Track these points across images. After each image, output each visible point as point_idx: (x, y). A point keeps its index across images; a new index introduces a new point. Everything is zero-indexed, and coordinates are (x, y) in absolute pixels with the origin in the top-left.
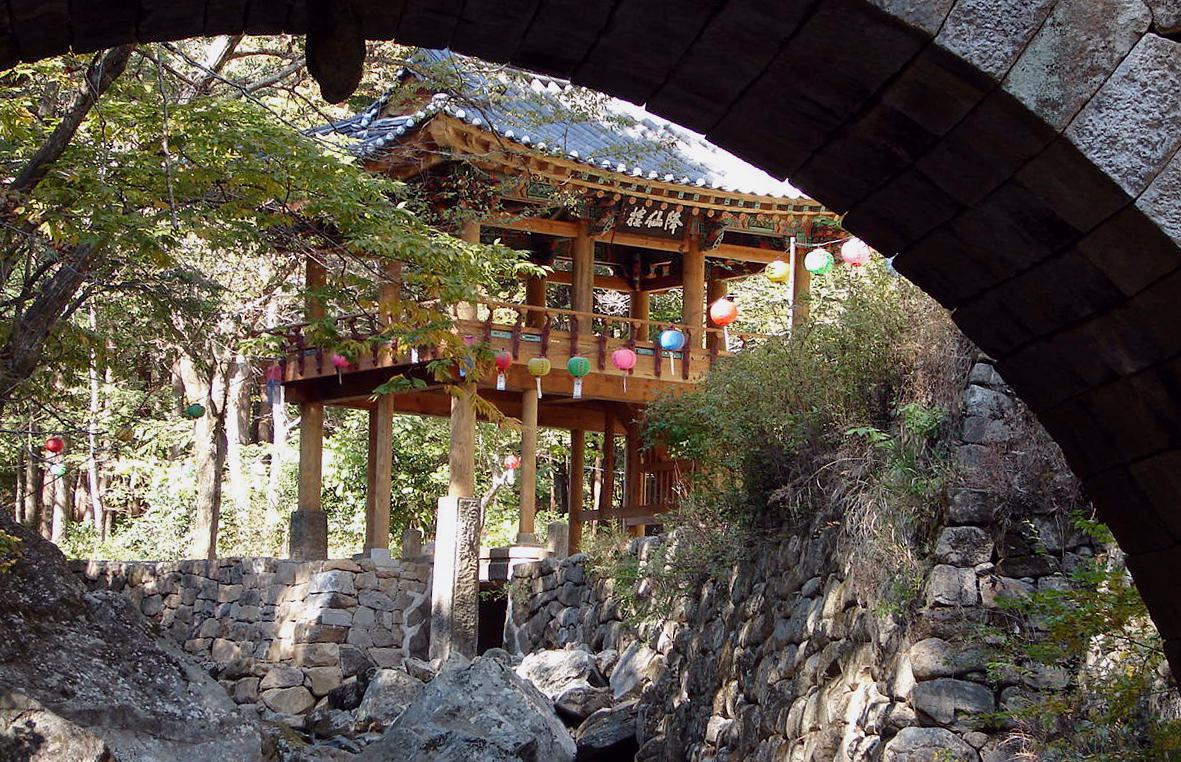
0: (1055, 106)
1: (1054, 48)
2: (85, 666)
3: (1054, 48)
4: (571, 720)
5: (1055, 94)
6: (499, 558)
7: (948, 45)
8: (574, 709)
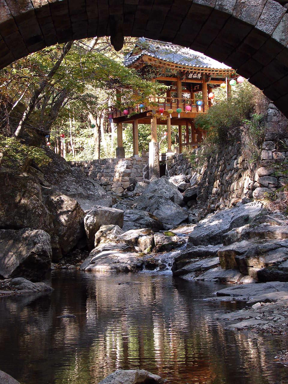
0: (284, 40)
1: (283, 27)
2: (71, 184)
3: (283, 27)
4: (182, 191)
5: (284, 37)
6: (164, 155)
7: (258, 28)
8: (182, 188)
